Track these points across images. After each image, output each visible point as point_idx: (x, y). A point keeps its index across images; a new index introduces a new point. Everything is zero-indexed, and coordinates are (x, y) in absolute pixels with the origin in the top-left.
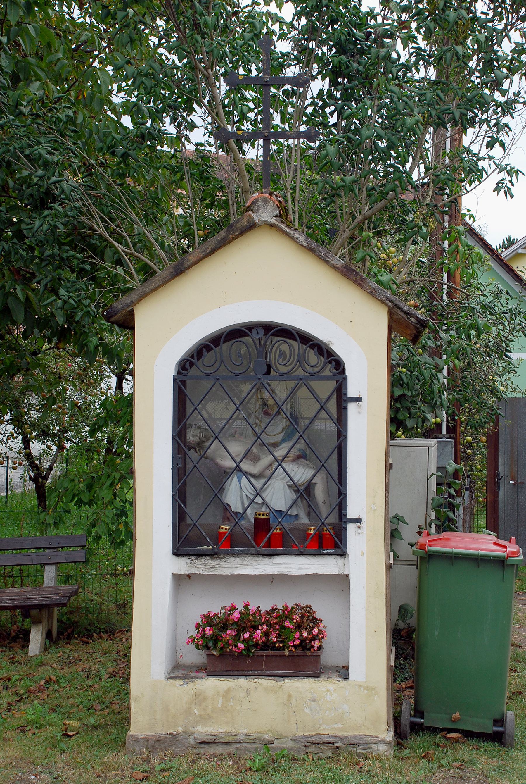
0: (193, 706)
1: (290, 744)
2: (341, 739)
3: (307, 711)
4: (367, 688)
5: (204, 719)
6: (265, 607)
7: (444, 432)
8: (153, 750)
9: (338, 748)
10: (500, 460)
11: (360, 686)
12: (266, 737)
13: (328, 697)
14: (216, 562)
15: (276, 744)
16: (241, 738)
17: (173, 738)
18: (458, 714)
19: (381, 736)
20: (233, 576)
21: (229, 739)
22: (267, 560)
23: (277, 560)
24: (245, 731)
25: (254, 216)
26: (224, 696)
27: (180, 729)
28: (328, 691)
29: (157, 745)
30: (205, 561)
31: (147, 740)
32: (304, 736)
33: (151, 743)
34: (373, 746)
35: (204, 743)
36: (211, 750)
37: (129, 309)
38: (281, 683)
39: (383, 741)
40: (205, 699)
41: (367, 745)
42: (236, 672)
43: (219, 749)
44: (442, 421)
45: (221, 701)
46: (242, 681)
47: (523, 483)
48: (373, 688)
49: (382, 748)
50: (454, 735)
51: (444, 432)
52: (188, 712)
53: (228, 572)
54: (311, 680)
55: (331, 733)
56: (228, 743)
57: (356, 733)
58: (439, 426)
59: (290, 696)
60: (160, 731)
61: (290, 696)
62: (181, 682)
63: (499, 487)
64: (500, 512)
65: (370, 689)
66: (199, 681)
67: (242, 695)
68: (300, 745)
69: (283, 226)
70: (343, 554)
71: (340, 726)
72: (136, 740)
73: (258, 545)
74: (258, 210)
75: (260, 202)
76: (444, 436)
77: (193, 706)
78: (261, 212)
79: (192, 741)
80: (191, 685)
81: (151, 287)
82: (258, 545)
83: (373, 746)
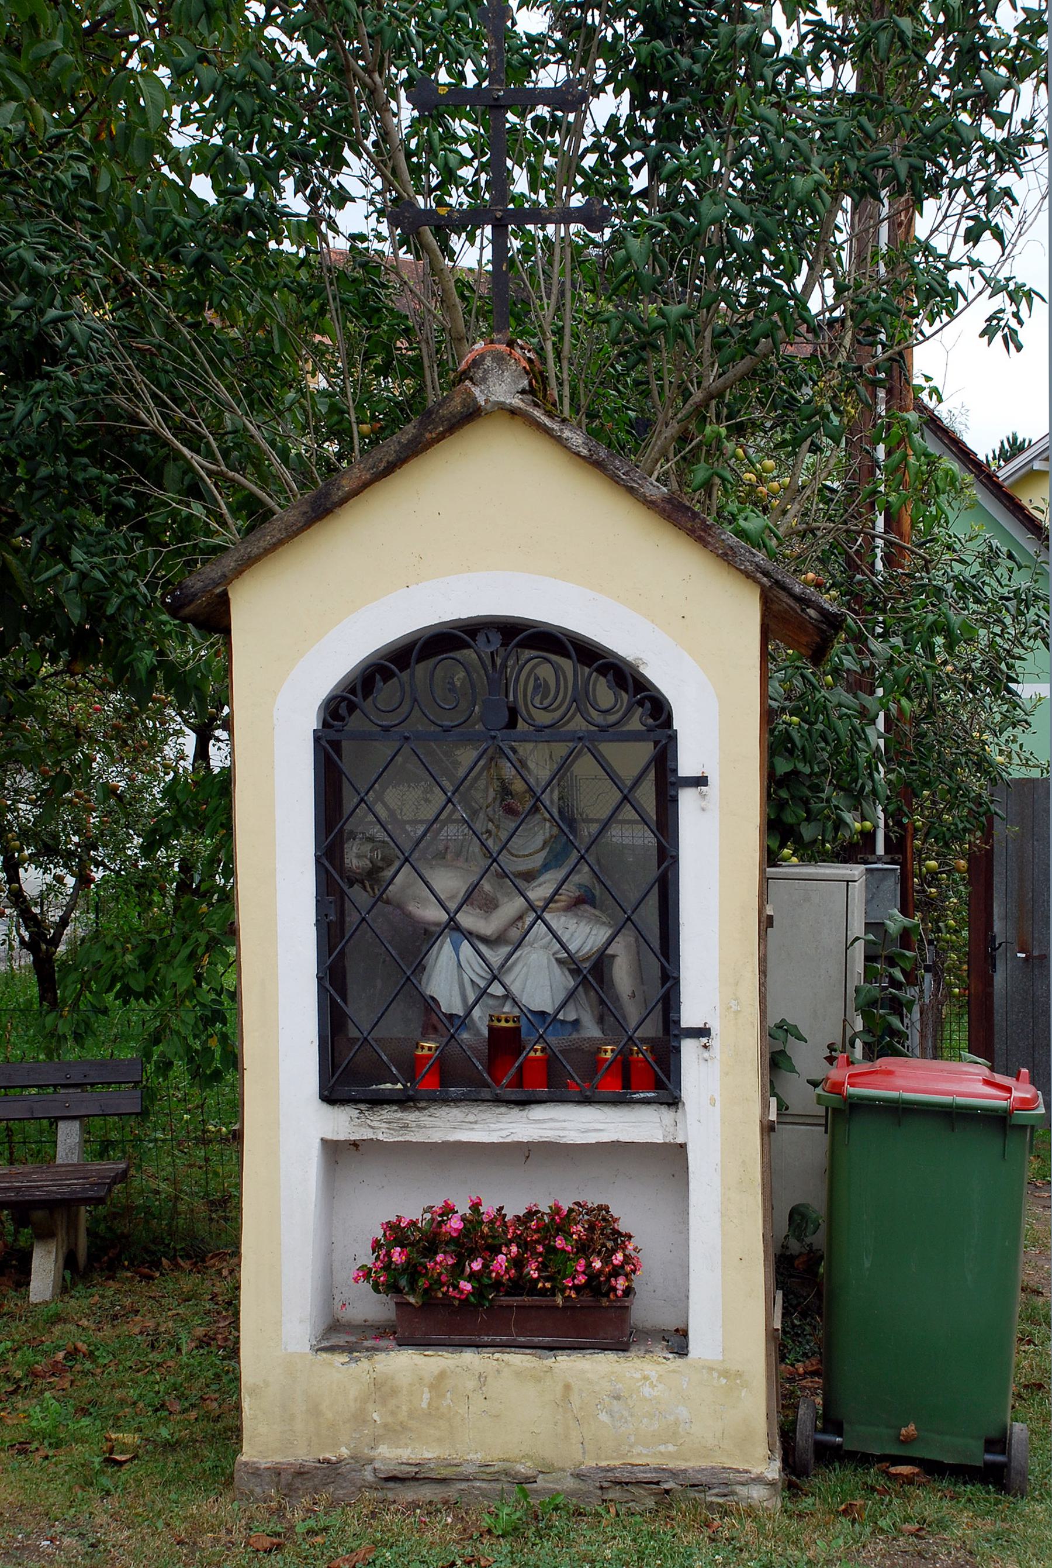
0: (370, 1407)
1: (571, 1484)
2: (674, 1474)
3: (604, 1417)
4: (725, 1374)
5: (394, 1432)
6: (514, 1209)
7: (880, 849)
9: (667, 1492)
10: (997, 910)
11: (711, 1369)
12: (521, 1468)
13: (647, 1391)
15: (541, 1483)
16: (469, 1470)
17: (331, 1469)
18: (912, 1427)
19: (757, 1470)
21: (445, 1473)
22: (515, 1113)
23: (538, 1112)
24: (478, 1457)
26: (432, 1387)
27: (344, 1452)
28: (645, 1378)
29: (298, 1483)
30: (389, 1113)
31: (277, 1471)
32: (599, 1468)
33: (285, 1478)
34: (738, 1489)
36: (409, 1494)
38: (549, 1362)
39: (759, 1480)
40: (394, 1392)
42: (456, 1338)
43: (426, 1493)
44: (876, 827)
45: (426, 1396)
46: (469, 1357)
48: (739, 1374)
49: (758, 1493)
50: (905, 1470)
51: (880, 849)
52: (360, 1418)
54: (611, 1356)
55: (654, 1462)
56: (443, 1481)
57: (704, 1464)
58: (869, 837)
59: (567, 1387)
60: (303, 1454)
61: (567, 1387)
63: (994, 966)
64: (998, 1018)
65: (732, 1376)
66: (380, 1357)
67: (471, 1384)
71: (671, 1448)
72: (255, 1472)
76: (879, 860)
77: (370, 1407)
79: (368, 1475)
80: (365, 1364)
83: (738, 1489)
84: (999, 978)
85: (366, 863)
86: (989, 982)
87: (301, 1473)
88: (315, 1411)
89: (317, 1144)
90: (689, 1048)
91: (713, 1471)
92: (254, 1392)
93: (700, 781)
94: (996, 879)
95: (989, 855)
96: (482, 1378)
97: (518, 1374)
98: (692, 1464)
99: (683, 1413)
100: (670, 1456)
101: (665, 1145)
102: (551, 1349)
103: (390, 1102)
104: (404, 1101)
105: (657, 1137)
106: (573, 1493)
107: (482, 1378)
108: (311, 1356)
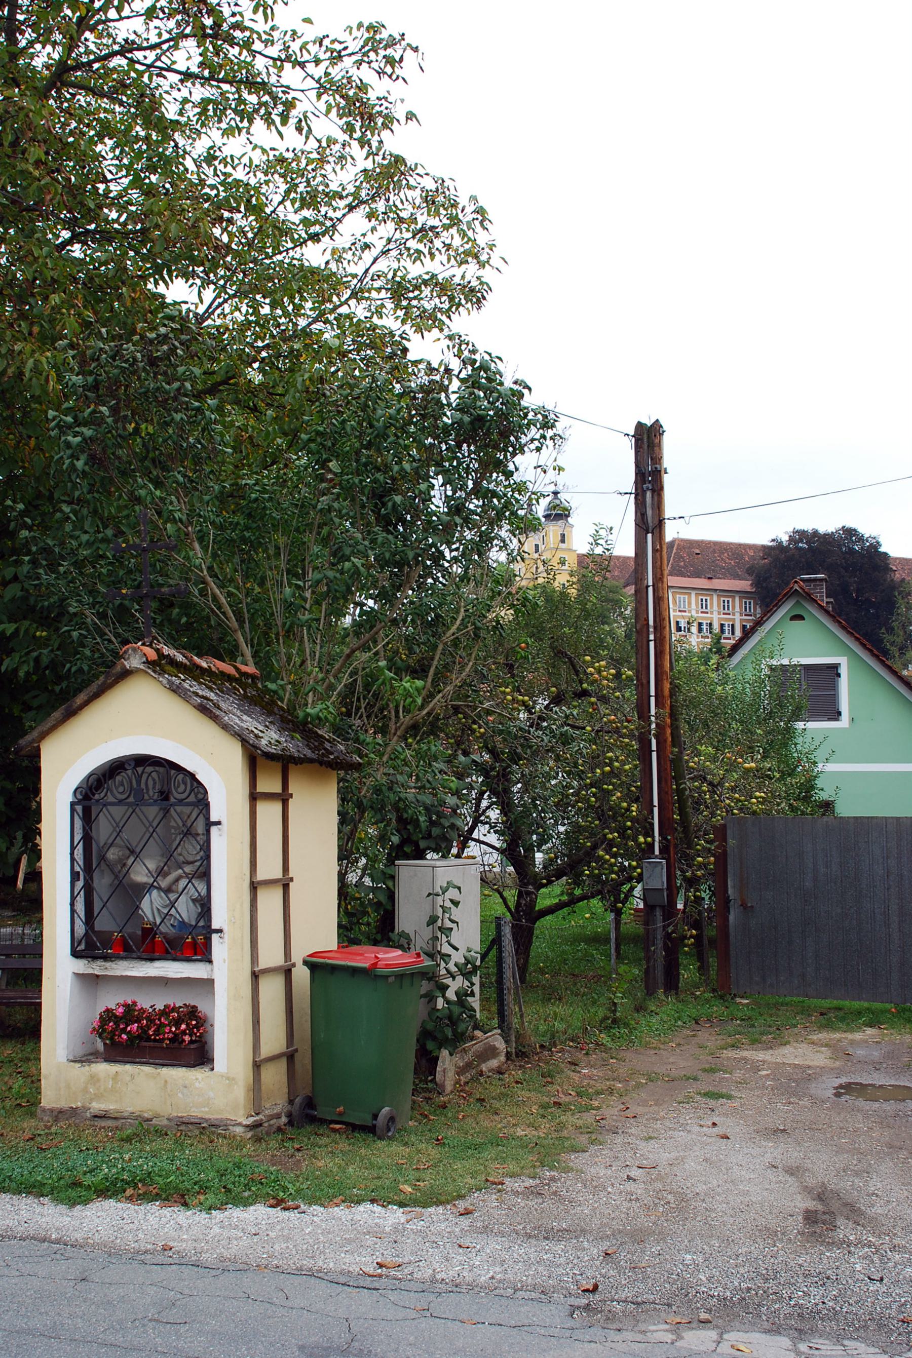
0: (89, 1086)
1: (166, 1122)
2: (206, 1120)
3: (180, 1095)
4: (228, 1078)
5: (98, 1097)
6: (160, 1006)
7: (657, 852)
8: (56, 1120)
9: (203, 1128)
10: (730, 883)
11: (222, 1076)
12: (146, 1115)
13: (197, 1084)
14: (108, 964)
15: (154, 1121)
16: (126, 1114)
17: (74, 1111)
18: (342, 1108)
19: (239, 1120)
20: (127, 976)
21: (116, 1115)
22: (148, 964)
23: (157, 964)
24: (130, 1109)
25: (126, 663)
26: (113, 1079)
27: (79, 1104)
28: (197, 1079)
29: (60, 1115)
30: (100, 963)
31: (51, 1110)
32: (177, 1117)
33: (55, 1113)
34: (231, 1128)
35: (96, 1116)
36: (104, 1123)
37: (36, 745)
38: (159, 1070)
39: (240, 1124)
40: (99, 1080)
41: (226, 1127)
42: (126, 1059)
43: (110, 1123)
44: (654, 840)
45: (111, 1083)
46: (128, 1067)
47: (752, 907)
48: (233, 1079)
49: (239, 1130)
50: (338, 1126)
51: (657, 852)
52: (85, 1090)
53: (118, 973)
54: (184, 1069)
55: (200, 1115)
56: (115, 1118)
57: (219, 1117)
58: (651, 846)
59: (166, 1082)
60: (63, 1104)
61: (166, 1082)
62: (79, 1065)
63: (729, 912)
64: (731, 938)
65: (231, 1080)
66: (93, 1065)
67: (128, 1078)
68: (173, 1124)
69: (149, 671)
70: (210, 961)
71: (207, 1109)
72: (44, 1110)
73: (139, 950)
74: (129, 658)
75: (130, 651)
76: (656, 857)
77: (89, 1086)
78: (131, 658)
79: (88, 1115)
80: (87, 1068)
81: (50, 724)
82: (139, 950)
83: (231, 1128)
84: (731, 918)
85: (116, 857)
86: (727, 919)
87: (61, 1112)
88: (68, 1087)
89: (70, 974)
90: (215, 937)
91: (222, 1120)
92: (45, 1078)
93: (219, 823)
94: (729, 867)
95: (725, 853)
96: (133, 1077)
97: (147, 1075)
98: (213, 1116)
99: (211, 1094)
100: (206, 1113)
101: (207, 979)
102: (163, 1065)
103: (101, 958)
104: (106, 958)
105: (205, 976)
106: (166, 1126)
107: (133, 1077)
108: (67, 1063)
